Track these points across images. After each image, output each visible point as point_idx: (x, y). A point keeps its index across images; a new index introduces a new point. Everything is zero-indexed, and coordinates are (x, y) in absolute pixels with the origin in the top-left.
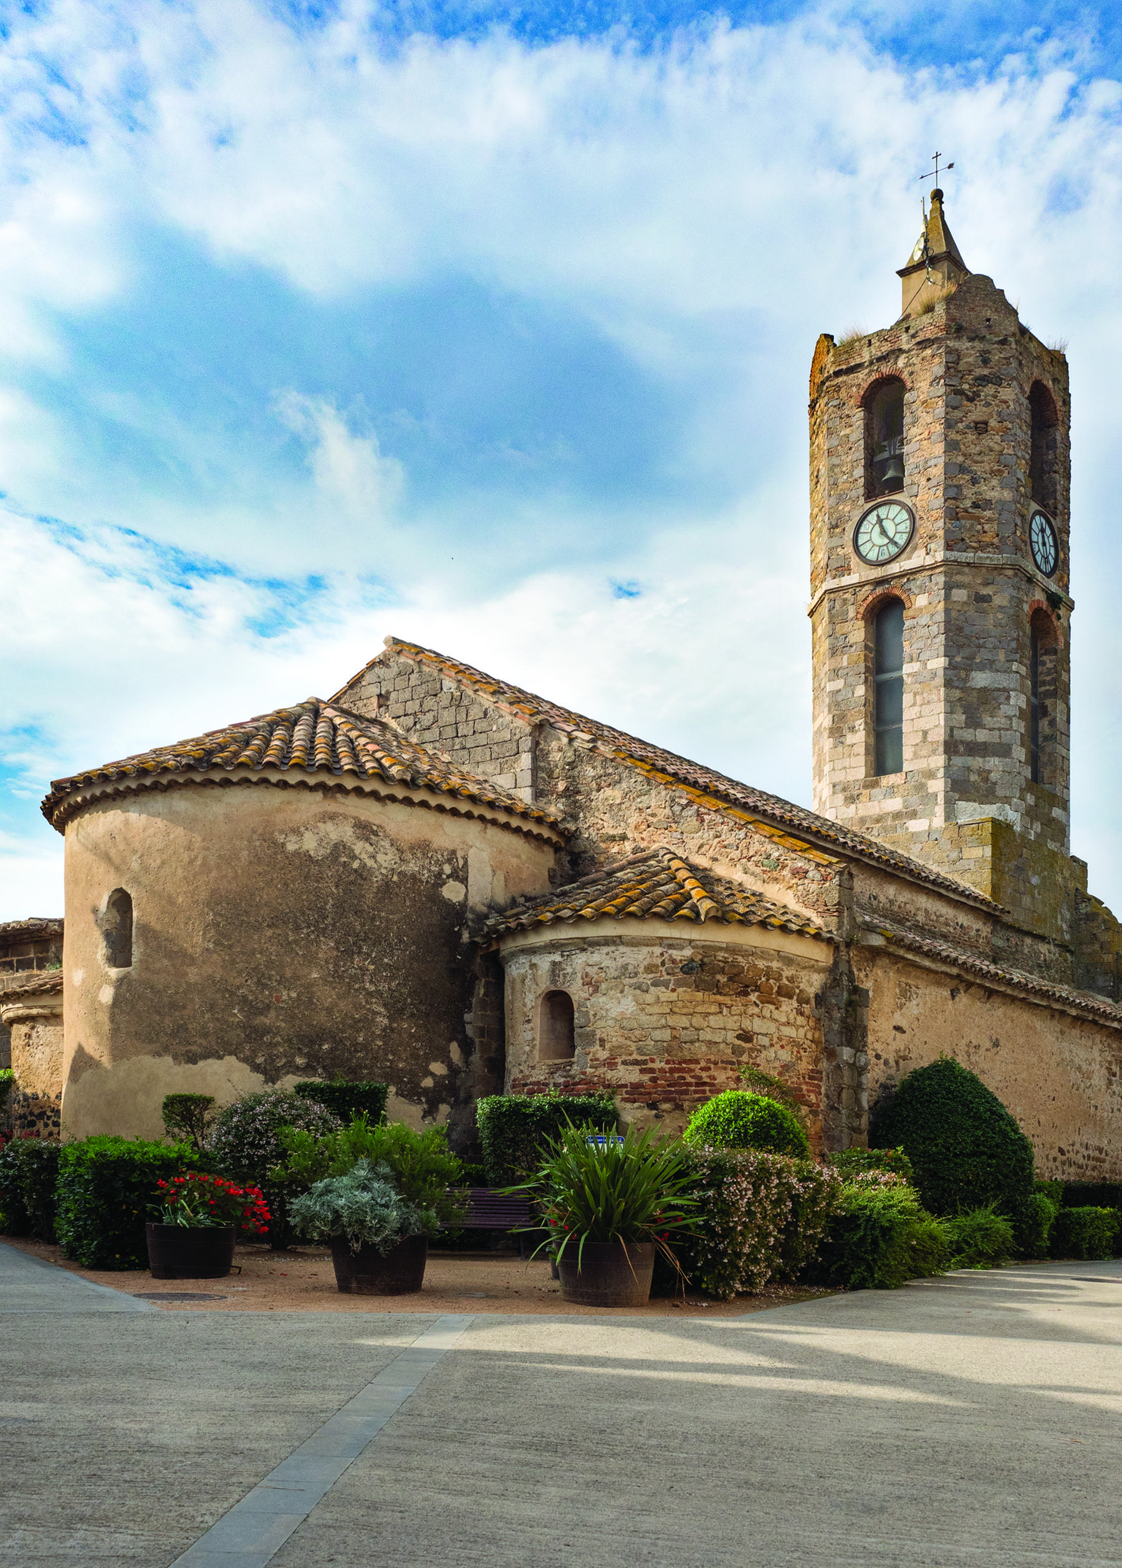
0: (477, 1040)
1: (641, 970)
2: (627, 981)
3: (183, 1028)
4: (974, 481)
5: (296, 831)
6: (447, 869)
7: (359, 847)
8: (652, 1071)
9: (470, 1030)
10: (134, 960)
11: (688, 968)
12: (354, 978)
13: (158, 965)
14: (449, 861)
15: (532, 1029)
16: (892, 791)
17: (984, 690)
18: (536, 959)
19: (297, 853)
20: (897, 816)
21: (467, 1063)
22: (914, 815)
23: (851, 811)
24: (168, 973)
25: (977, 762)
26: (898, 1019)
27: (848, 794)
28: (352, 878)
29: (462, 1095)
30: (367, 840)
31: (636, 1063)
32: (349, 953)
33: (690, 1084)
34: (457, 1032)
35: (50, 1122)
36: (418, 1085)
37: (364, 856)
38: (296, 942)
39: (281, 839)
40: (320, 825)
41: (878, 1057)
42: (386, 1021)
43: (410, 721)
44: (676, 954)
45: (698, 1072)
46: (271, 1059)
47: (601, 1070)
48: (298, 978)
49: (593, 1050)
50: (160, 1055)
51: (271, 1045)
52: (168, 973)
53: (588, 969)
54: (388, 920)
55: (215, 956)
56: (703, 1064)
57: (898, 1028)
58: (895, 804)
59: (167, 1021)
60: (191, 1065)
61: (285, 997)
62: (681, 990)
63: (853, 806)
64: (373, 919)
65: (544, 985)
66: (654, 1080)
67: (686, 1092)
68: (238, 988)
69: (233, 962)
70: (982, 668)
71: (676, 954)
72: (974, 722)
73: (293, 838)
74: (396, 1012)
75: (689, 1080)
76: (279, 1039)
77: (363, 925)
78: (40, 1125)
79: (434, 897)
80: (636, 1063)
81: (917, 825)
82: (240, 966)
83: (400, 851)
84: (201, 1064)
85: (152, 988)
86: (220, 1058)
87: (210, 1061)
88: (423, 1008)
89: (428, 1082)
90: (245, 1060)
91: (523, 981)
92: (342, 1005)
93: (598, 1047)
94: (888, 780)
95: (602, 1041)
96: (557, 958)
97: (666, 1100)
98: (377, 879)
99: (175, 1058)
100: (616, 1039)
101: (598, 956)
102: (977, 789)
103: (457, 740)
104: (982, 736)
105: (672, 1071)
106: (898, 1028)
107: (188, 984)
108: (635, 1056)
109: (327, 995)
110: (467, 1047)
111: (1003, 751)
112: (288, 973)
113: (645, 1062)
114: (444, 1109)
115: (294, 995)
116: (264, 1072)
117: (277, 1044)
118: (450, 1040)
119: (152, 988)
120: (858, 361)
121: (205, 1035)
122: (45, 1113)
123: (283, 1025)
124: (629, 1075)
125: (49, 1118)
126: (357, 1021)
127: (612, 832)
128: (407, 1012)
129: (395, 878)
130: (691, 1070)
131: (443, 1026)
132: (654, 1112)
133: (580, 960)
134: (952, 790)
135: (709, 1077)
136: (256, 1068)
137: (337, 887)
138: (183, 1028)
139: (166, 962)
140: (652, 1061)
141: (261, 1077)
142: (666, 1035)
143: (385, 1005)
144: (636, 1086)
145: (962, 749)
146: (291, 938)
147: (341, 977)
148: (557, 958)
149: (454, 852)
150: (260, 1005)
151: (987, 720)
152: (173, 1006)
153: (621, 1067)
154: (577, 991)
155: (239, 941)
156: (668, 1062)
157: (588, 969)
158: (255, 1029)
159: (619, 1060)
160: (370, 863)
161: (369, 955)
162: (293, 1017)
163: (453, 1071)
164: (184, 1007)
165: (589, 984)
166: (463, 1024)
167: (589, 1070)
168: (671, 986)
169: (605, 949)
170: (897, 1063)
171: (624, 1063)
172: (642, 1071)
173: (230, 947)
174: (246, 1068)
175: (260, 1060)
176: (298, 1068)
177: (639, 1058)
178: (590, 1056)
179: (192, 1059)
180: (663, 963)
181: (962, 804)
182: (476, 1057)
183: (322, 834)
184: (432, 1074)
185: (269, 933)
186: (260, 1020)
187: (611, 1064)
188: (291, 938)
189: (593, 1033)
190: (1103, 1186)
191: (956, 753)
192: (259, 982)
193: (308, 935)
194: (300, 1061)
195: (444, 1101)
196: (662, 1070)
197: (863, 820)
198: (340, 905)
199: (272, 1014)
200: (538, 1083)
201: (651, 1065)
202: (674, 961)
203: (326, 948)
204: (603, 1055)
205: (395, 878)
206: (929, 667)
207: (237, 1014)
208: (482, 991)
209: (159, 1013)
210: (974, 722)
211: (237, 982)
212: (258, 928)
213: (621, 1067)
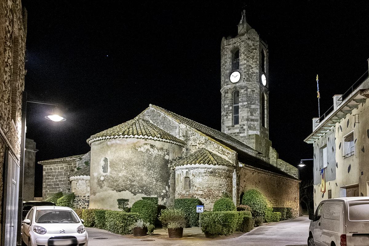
0: (171, 185)
1: (203, 173)
2: (200, 175)
3: (118, 185)
4: (252, 68)
5: (140, 147)
6: (166, 153)
7: (151, 150)
8: (205, 192)
9: (170, 184)
10: (108, 171)
11: (211, 172)
12: (150, 175)
13: (113, 173)
14: (166, 151)
15: (182, 184)
16: (236, 128)
17: (253, 109)
18: (183, 170)
19: (140, 151)
20: (238, 133)
21: (169, 190)
22: (241, 133)
23: (230, 132)
24: (115, 174)
25: (252, 123)
26: (244, 179)
27: (229, 128)
28: (150, 155)
29: (168, 196)
30: (152, 148)
31: (202, 190)
32: (149, 170)
33: (211, 194)
34: (167, 184)
35: (82, 202)
36: (161, 195)
37: (152, 151)
38: (140, 168)
39: (137, 148)
40: (144, 146)
41: (241, 187)
42: (155, 183)
43: (155, 121)
44: (209, 170)
45: (213, 192)
46: (135, 191)
47: (195, 192)
48: (140, 175)
49: (194, 188)
50: (113, 190)
51: (135, 188)
52: (115, 174)
53: (193, 173)
54: (156, 163)
55: (125, 171)
56: (213, 190)
57: (244, 181)
58: (237, 131)
59: (115, 184)
60: (119, 192)
61: (138, 179)
62: (210, 177)
63: (229, 131)
64: (153, 163)
65: (185, 175)
66: (205, 193)
67: (211, 195)
68: (129, 177)
69: (128, 172)
70: (253, 104)
71: (209, 170)
72: (252, 115)
73: (139, 148)
74: (157, 181)
75: (211, 193)
76: (136, 187)
77: (151, 164)
78: (79, 202)
79: (164, 159)
80: (202, 190)
81: (241, 135)
82: (129, 173)
83: (158, 150)
84: (121, 192)
85: (112, 177)
86: (125, 191)
87: (123, 191)
88: (162, 180)
89: (162, 194)
90: (130, 191)
91: (180, 174)
92: (148, 180)
93: (195, 187)
94: (236, 126)
95: (196, 186)
96: (187, 170)
97: (207, 197)
98: (154, 156)
99: (116, 191)
100: (198, 186)
101: (195, 170)
102: (253, 128)
103: (164, 126)
104: (253, 118)
105: (208, 192)
106: (244, 181)
107: (119, 176)
108: (202, 189)
109: (145, 178)
110: (169, 187)
111: (257, 120)
112: (138, 174)
113: (203, 190)
114: (165, 199)
115: (139, 178)
116: (134, 193)
117: (136, 188)
118: (166, 186)
119: (112, 177)
120: (230, 43)
121: (122, 187)
122: (80, 200)
123: (137, 184)
124: (201, 193)
125: (81, 201)
126: (150, 183)
127: (194, 145)
128: (159, 181)
129: (157, 155)
130: (211, 192)
131: (165, 183)
132: (205, 199)
133: (192, 171)
134: (248, 128)
135: (21, 86)
136: (132, 193)
137: (147, 157)
138: (118, 185)
139: (115, 172)
140: (205, 190)
141: (133, 194)
142: (207, 185)
143: (155, 180)
144: (202, 195)
145: (250, 120)
146: (139, 167)
147: (148, 175)
148: (187, 170)
149: (167, 150)
150: (133, 180)
151: (254, 114)
152: (116, 181)
153: (199, 191)
154: (191, 177)
155: (129, 168)
156: (207, 190)
157: (193, 173)
158: (132, 185)
159: (199, 190)
160: (153, 153)
161: (152, 170)
162: (139, 183)
163: (167, 192)
164: (118, 181)
165: (193, 175)
166: (168, 182)
167: (193, 192)
168: (208, 176)
169: (196, 169)
170: (244, 187)
171: (200, 190)
172: (203, 192)
173: (127, 169)
174: (130, 193)
175: (133, 191)
176: (140, 192)
177: (203, 189)
178: (193, 189)
179: (120, 191)
180: (207, 172)
181: (250, 131)
182: (170, 189)
183: (145, 147)
184: (163, 192)
185: (135, 166)
186: (132, 183)
187: (197, 190)
188: (139, 167)
189: (194, 185)
190: (168, 110)
191: (249, 121)
192: (133, 176)
193: (142, 167)
194: (140, 191)
195: (165, 197)
196: (206, 192)
197: (231, 134)
198: (147, 161)
199: (135, 182)
200: (183, 194)
201: (204, 191)
202: (208, 171)
203: (145, 169)
204: (196, 189)
205: (157, 155)
206: (244, 104)
207: (129, 182)
208: (172, 176)
209: (113, 182)
210: (252, 115)
211: (129, 176)
212: (133, 165)
213: (199, 191)
